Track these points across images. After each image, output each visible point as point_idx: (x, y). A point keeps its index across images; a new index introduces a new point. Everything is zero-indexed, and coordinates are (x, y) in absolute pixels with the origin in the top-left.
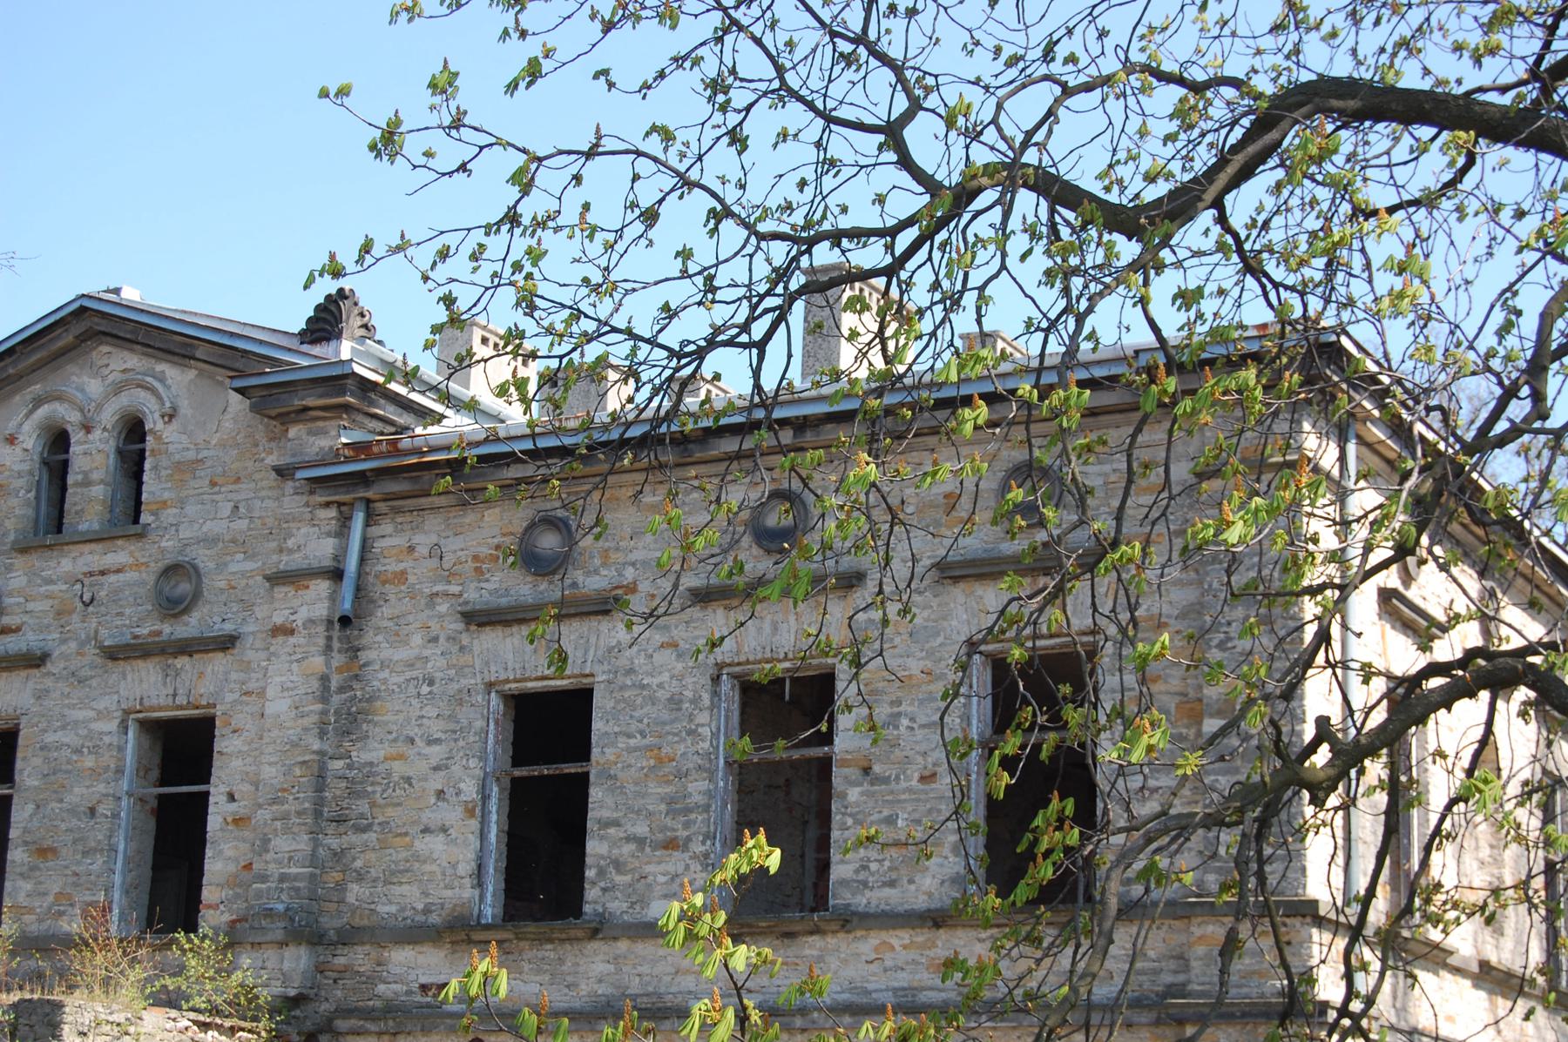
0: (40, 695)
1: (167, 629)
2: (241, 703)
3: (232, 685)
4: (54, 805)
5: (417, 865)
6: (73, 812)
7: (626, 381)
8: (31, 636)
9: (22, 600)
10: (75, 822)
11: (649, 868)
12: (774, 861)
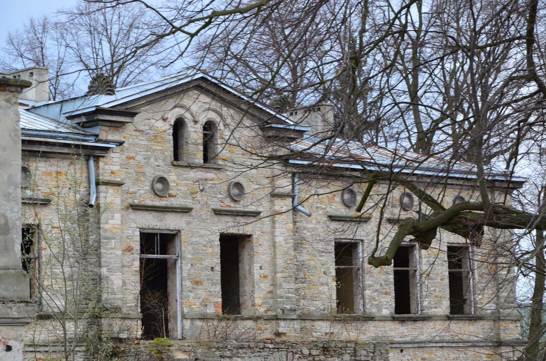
0: (189, 223)
2: (262, 236)
3: (258, 229)
4: (199, 265)
5: (320, 295)
6: (206, 268)
8: (181, 199)
9: (175, 184)
10: (207, 272)
11: (382, 300)
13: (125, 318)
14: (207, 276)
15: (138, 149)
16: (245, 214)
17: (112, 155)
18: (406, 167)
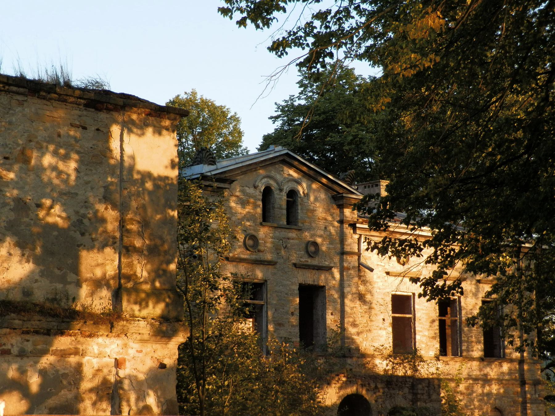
1: (309, 260)
4: (281, 310)
7: (200, 257)
12: (392, 36)
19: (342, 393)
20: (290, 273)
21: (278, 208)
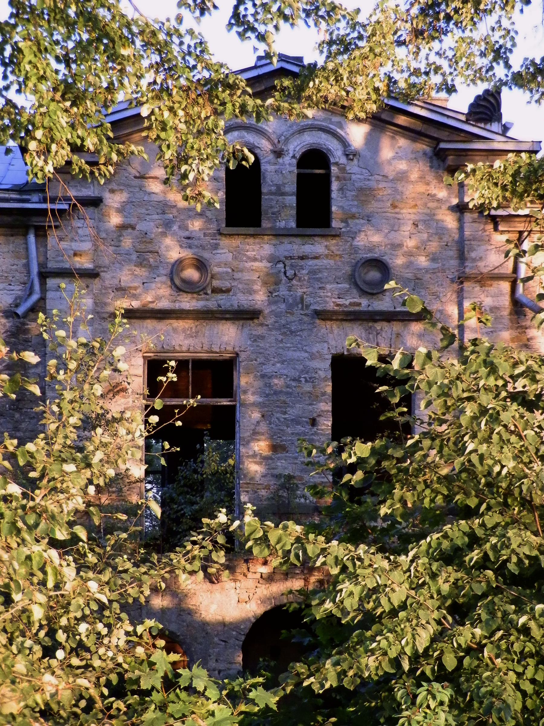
6: (296, 421)
9: (229, 270)
13: (279, 235)
14: (298, 434)
15: (143, 211)
16: (390, 317)
17: (77, 223)
18: (125, 324)
19: (278, 588)
20: (305, 333)
21: (271, 193)
